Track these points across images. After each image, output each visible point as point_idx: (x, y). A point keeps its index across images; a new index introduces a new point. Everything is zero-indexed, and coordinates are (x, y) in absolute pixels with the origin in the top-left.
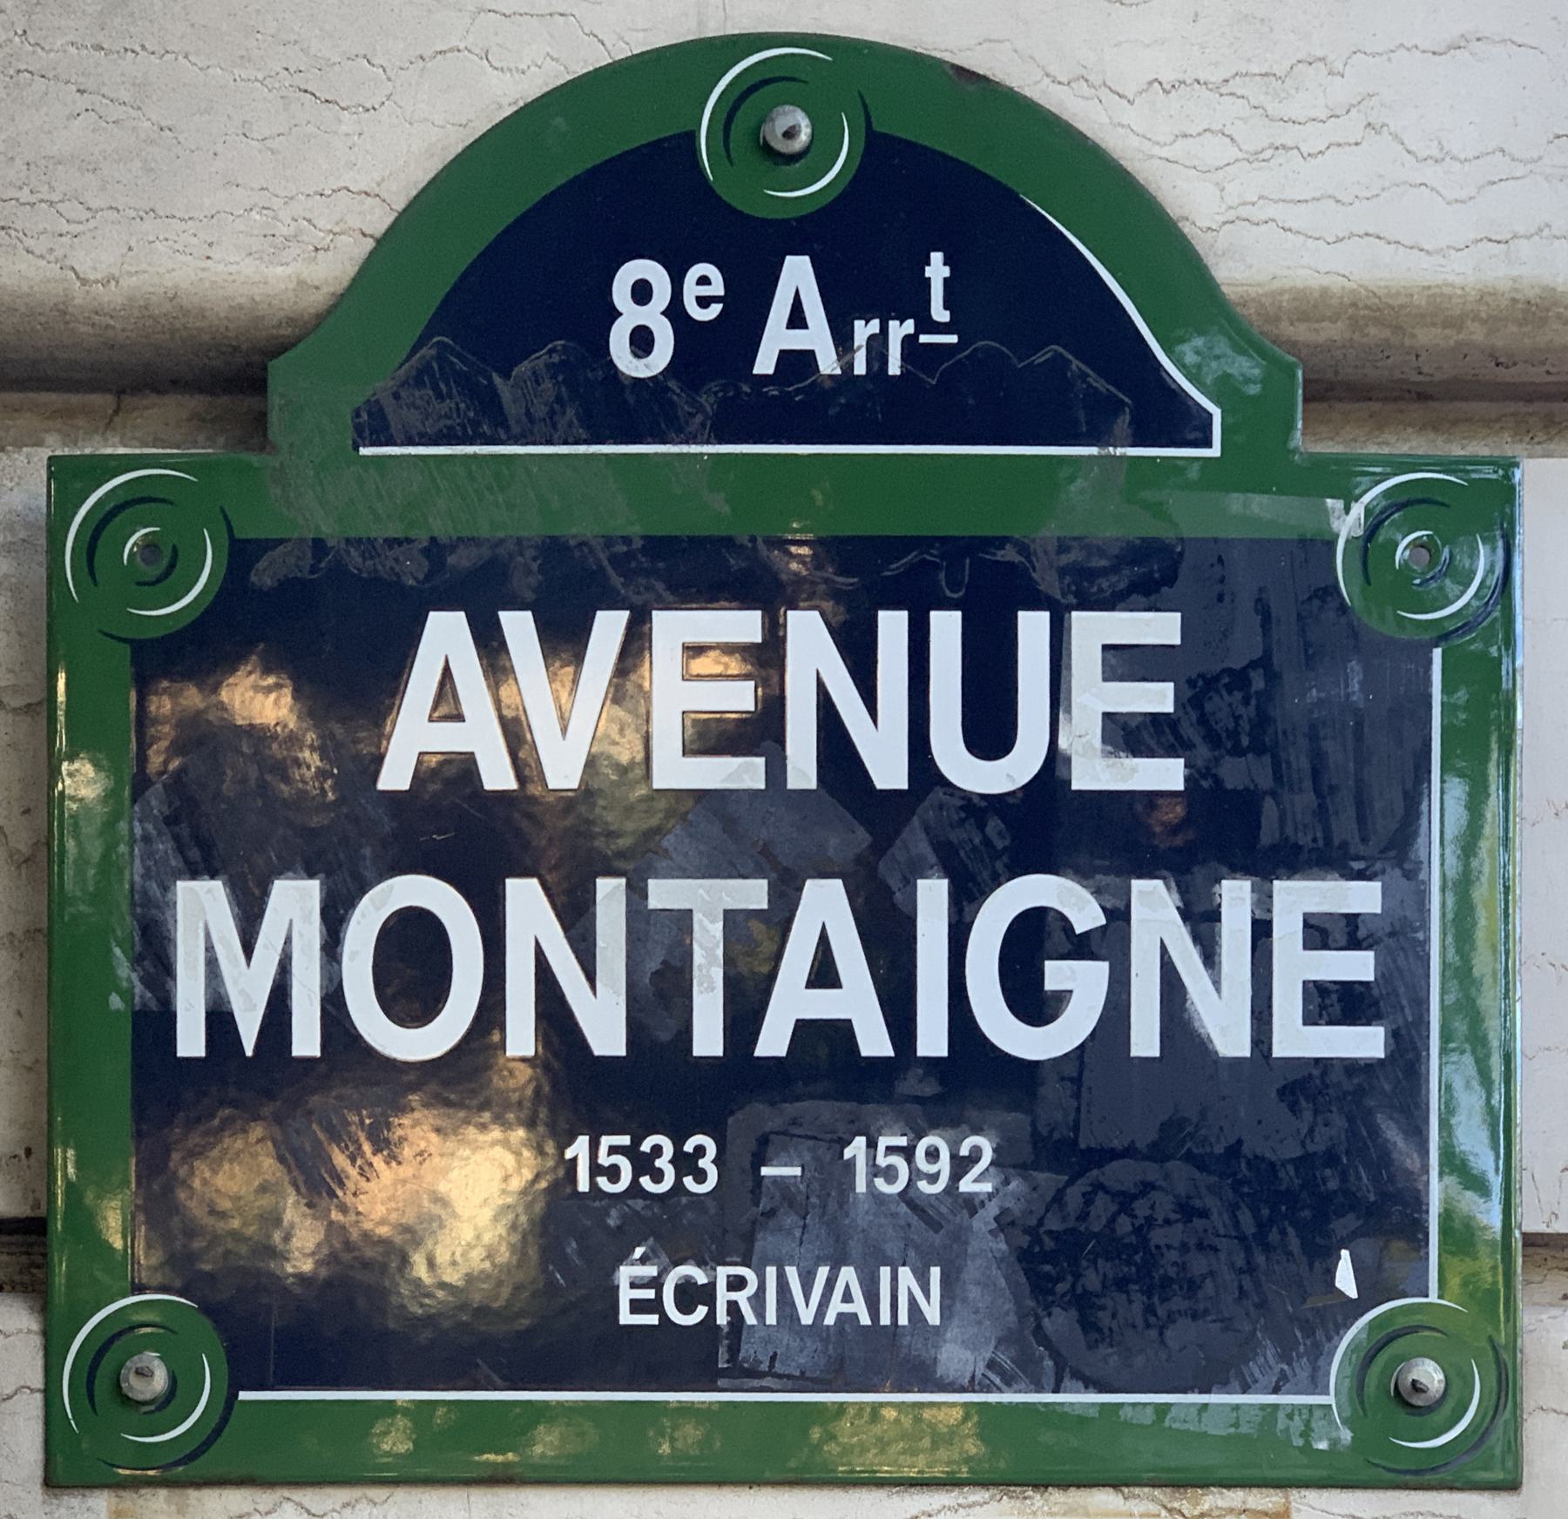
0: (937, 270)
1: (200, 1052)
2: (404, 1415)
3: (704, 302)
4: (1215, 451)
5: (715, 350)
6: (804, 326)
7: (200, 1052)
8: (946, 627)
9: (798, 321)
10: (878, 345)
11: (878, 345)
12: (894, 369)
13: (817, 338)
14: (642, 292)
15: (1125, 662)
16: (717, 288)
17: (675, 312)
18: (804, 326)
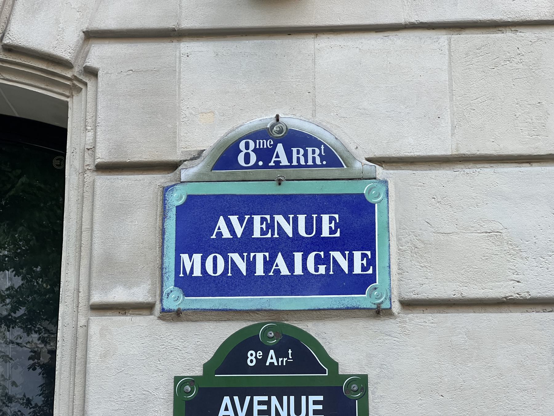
0: (290, 352)
1: (284, 397)
2: (50, 358)
3: (260, 356)
4: (327, 375)
5: (261, 362)
6: (228, 410)
7: (284, 397)
8: (292, 398)
9: (272, 358)
10: (282, 361)
11: (282, 361)
12: (284, 364)
13: (274, 360)
14: (252, 355)
15: (315, 403)
16: (261, 354)
17: (256, 357)
18: (228, 410)
